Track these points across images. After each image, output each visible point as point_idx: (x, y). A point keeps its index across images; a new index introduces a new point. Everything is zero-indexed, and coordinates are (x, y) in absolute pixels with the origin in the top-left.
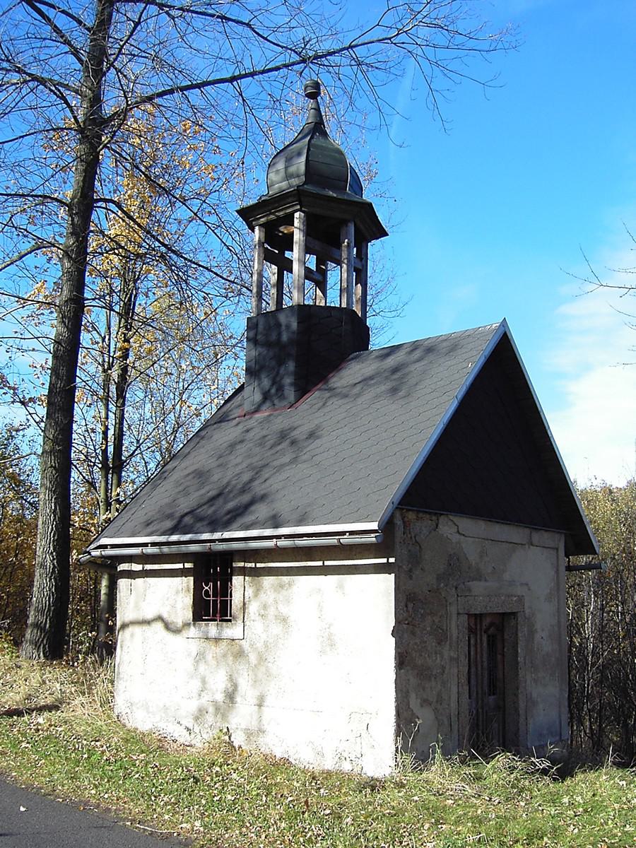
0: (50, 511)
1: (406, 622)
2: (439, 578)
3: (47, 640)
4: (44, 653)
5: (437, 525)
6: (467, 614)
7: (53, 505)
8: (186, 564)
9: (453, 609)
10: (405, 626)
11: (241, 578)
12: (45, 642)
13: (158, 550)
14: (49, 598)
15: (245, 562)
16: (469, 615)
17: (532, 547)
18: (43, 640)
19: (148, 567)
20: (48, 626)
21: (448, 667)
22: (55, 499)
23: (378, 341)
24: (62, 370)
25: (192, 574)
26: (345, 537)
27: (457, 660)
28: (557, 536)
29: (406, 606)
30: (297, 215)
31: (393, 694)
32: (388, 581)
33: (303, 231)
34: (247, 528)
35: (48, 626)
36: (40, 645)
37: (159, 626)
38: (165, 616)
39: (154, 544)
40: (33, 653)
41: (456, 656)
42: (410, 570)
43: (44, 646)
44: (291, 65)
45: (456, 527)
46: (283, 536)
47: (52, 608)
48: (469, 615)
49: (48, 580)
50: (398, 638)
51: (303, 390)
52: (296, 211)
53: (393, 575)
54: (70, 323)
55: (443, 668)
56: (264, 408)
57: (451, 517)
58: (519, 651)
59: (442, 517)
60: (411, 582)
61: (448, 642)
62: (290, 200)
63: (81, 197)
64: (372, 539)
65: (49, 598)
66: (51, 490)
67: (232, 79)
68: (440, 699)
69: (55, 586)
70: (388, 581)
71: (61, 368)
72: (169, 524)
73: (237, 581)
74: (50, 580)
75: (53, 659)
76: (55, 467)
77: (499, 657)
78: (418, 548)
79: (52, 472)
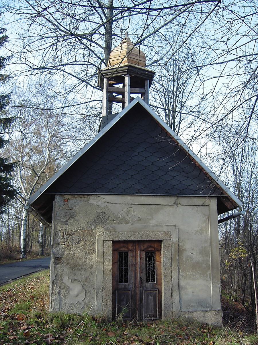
57: (102, 196)
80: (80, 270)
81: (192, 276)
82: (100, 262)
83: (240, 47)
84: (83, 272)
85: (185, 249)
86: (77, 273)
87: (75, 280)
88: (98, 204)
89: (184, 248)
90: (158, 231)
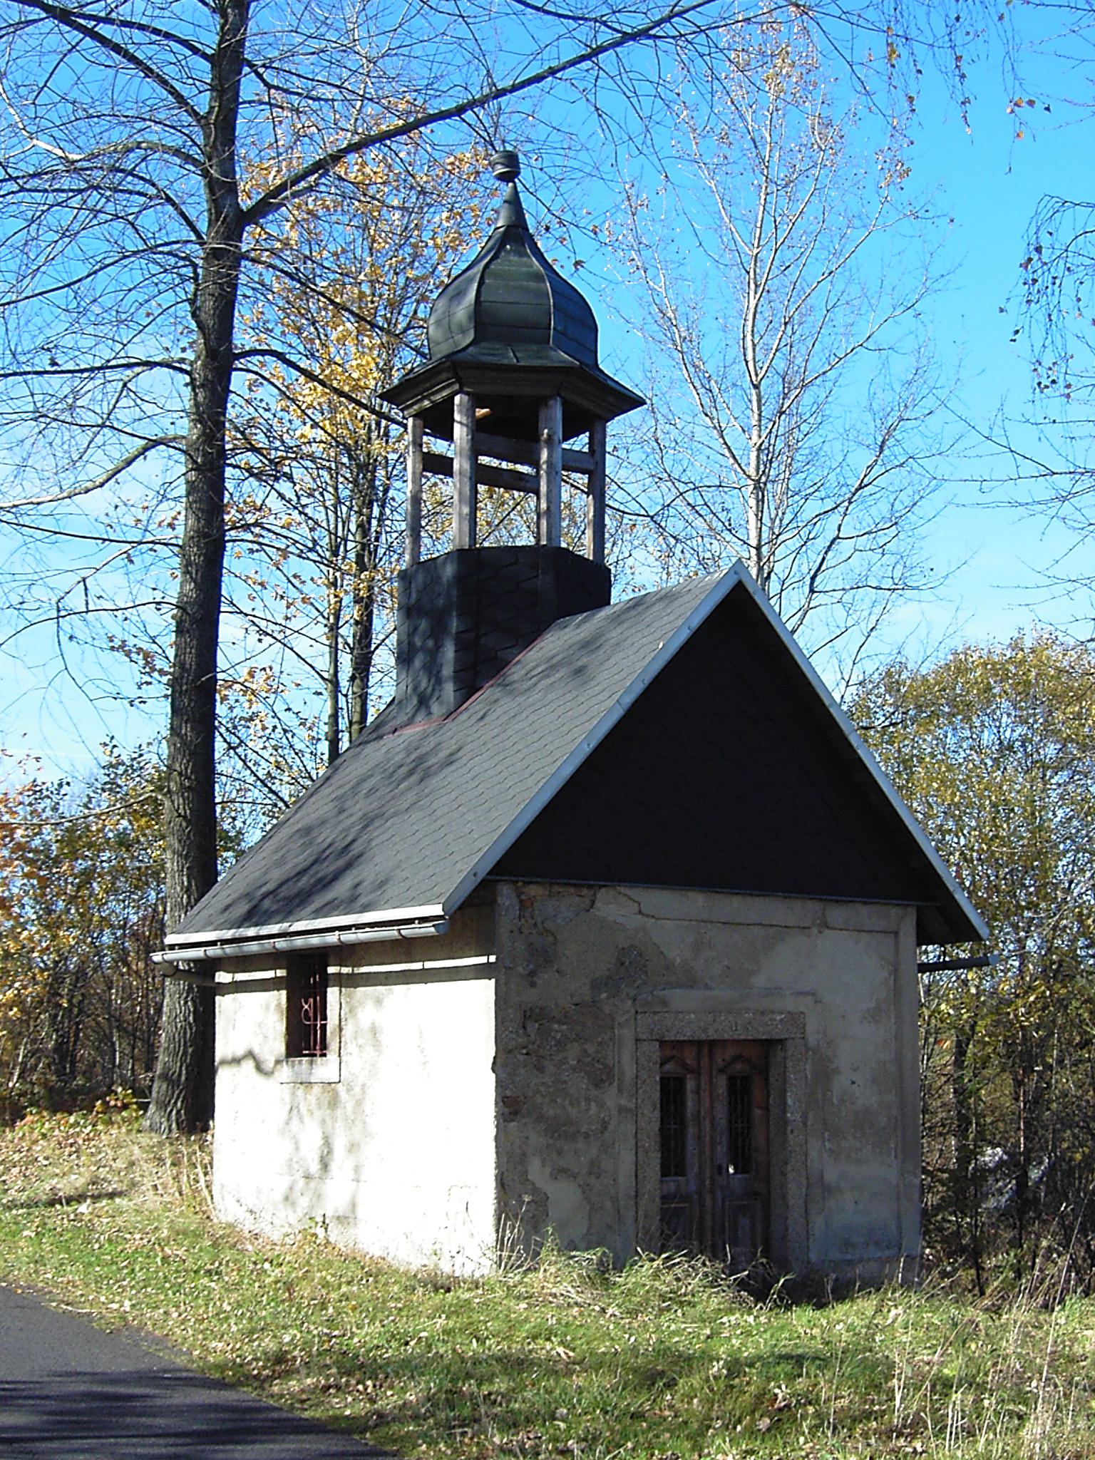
0: (182, 890)
1: (524, 1051)
2: (596, 985)
3: (182, 1102)
4: (178, 1124)
5: (593, 903)
6: (657, 1040)
7: (185, 879)
8: (278, 971)
9: (627, 1034)
10: (521, 1058)
11: (336, 989)
12: (179, 1104)
13: (237, 949)
14: (185, 1033)
15: (341, 966)
16: (662, 1043)
17: (826, 931)
18: (176, 1103)
19: (241, 977)
20: (183, 1078)
21: (614, 1122)
22: (188, 868)
23: (619, 594)
24: (190, 653)
25: (284, 985)
26: (413, 926)
27: (635, 1112)
28: (893, 912)
29: (524, 1027)
30: (457, 399)
31: (492, 1156)
32: (490, 984)
33: (467, 426)
34: (317, 914)
35: (183, 1078)
36: (171, 1111)
37: (249, 1065)
38: (257, 1051)
39: (225, 942)
40: (161, 1124)
41: (632, 1105)
42: (532, 974)
43: (178, 1112)
44: (559, 70)
45: (636, 905)
46: (354, 926)
47: (190, 1050)
48: (662, 1043)
49: (182, 1002)
50: (503, 1076)
51: (469, 686)
52: (456, 393)
53: (493, 980)
54: (200, 574)
55: (605, 1125)
56: (419, 718)
57: (622, 890)
58: (790, 1102)
59: (603, 890)
60: (534, 990)
61: (615, 1084)
62: (444, 376)
63: (207, 357)
64: (429, 929)
65: (185, 1033)
66: (181, 855)
67: (460, 111)
68: (595, 1169)
69: (194, 1013)
70: (485, 990)
71: (188, 650)
72: (243, 908)
73: (332, 993)
74: (186, 1003)
75: (191, 1132)
76: (185, 817)
77: (757, 1112)
78: (551, 939)
79: (181, 825)
80: (573, 1137)
81: (853, 1154)
82: (628, 1110)
83: (45, 86)
84: (580, 1145)
85: (837, 1067)
86: (566, 1148)
87: (562, 1171)
88: (619, 919)
89: (834, 1066)
90: (773, 1012)
